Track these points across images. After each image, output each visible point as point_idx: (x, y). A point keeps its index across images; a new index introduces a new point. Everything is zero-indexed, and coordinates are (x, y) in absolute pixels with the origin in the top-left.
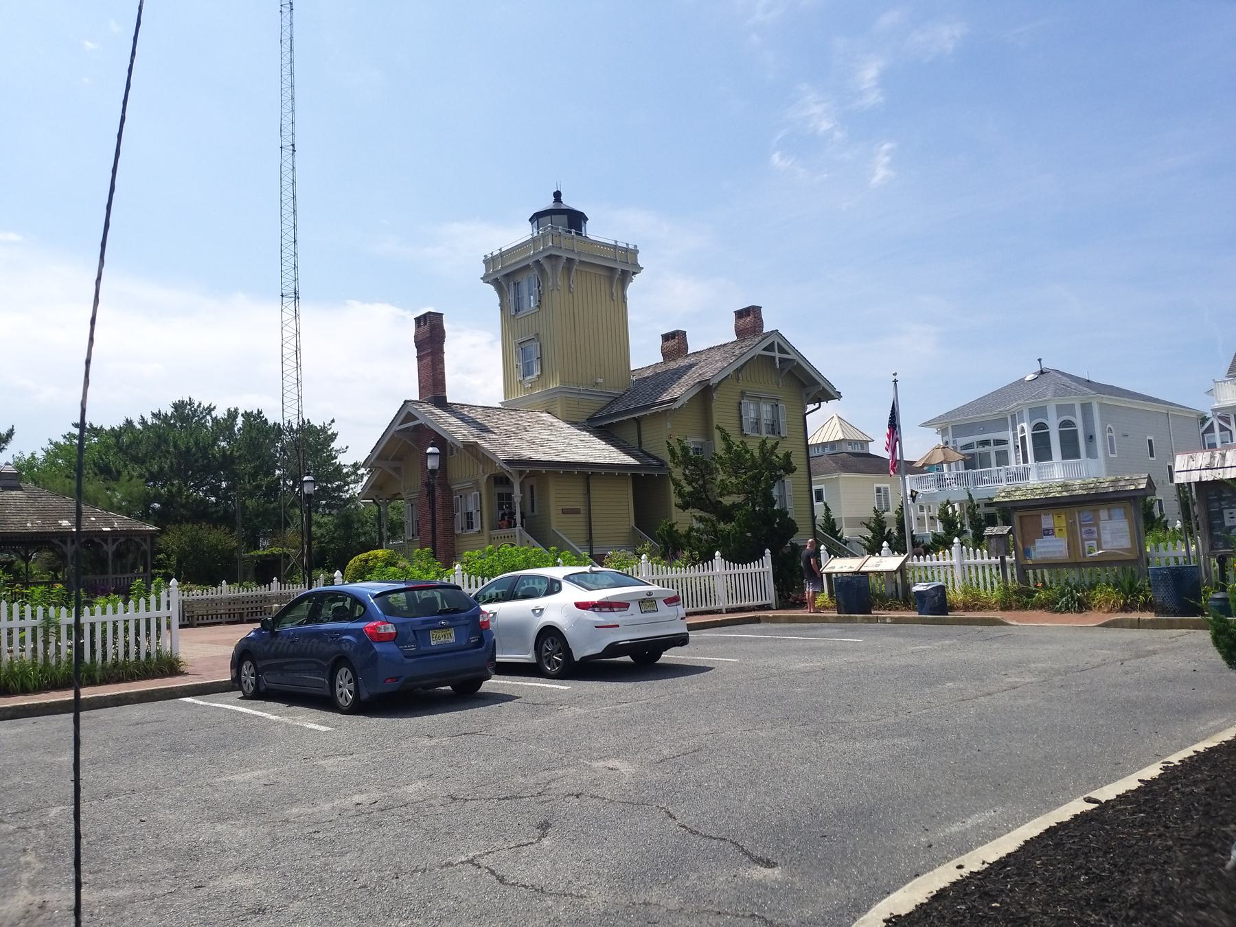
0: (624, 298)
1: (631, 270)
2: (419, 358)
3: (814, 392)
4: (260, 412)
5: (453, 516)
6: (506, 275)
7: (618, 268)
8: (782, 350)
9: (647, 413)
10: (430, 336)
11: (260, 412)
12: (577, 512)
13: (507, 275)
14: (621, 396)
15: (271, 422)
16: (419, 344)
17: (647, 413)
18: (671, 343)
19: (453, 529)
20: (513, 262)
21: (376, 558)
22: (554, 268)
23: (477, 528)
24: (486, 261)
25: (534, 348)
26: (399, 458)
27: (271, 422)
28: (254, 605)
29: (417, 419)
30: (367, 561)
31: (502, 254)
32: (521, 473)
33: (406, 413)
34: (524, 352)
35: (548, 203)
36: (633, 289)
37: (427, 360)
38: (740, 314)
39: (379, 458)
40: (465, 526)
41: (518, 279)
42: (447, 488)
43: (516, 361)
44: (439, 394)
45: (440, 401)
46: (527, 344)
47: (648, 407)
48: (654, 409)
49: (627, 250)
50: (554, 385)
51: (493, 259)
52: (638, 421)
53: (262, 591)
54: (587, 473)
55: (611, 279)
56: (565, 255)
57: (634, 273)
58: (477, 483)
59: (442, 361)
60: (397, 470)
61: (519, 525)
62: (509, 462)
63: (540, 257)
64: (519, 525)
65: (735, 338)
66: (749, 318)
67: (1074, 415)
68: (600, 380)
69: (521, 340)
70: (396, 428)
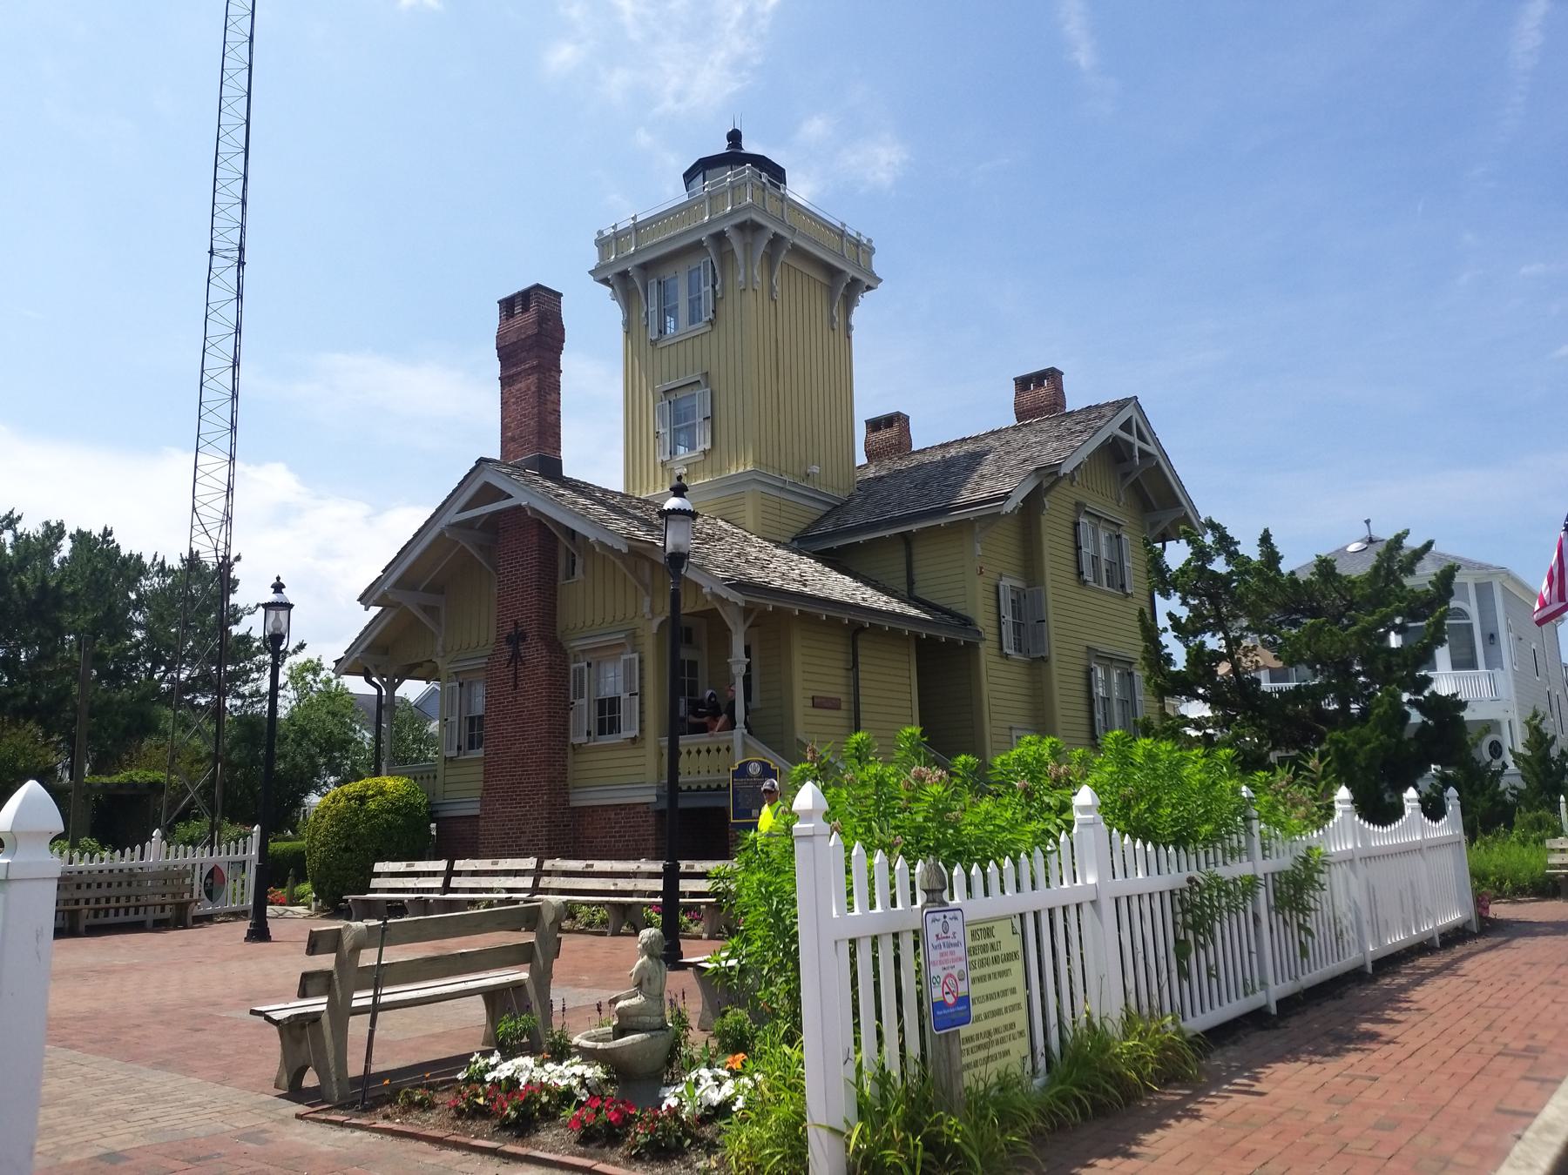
0: (849, 327)
1: (867, 282)
2: (506, 381)
3: (1166, 519)
4: (107, 533)
5: (568, 707)
6: (641, 271)
7: (838, 275)
8: (1141, 437)
9: (942, 521)
10: (530, 338)
11: (107, 533)
12: (834, 705)
13: (645, 267)
14: (845, 504)
15: (124, 552)
16: (507, 353)
17: (942, 521)
18: (884, 434)
19: (565, 733)
20: (658, 243)
21: (382, 792)
22: (747, 247)
23: (626, 734)
24: (603, 243)
25: (700, 402)
26: (436, 588)
27: (124, 552)
28: (104, 892)
29: (510, 496)
30: (362, 799)
31: (637, 227)
32: (747, 611)
33: (479, 485)
34: (671, 401)
35: (721, 147)
36: (865, 312)
37: (528, 383)
38: (1023, 383)
39: (400, 584)
40: (594, 729)
41: (667, 273)
42: (555, 647)
43: (655, 422)
44: (548, 452)
45: (550, 467)
46: (681, 394)
47: (944, 511)
48: (956, 516)
49: (858, 244)
50: (741, 467)
51: (617, 236)
52: (906, 538)
53: (126, 861)
54: (851, 627)
55: (831, 291)
56: (773, 228)
57: (869, 288)
58: (633, 636)
59: (556, 388)
60: (431, 611)
61: (740, 724)
62: (744, 586)
63: (726, 227)
64: (740, 724)
65: (1014, 422)
66: (1039, 392)
67: (1467, 601)
68: (816, 469)
69: (669, 385)
70: (453, 517)
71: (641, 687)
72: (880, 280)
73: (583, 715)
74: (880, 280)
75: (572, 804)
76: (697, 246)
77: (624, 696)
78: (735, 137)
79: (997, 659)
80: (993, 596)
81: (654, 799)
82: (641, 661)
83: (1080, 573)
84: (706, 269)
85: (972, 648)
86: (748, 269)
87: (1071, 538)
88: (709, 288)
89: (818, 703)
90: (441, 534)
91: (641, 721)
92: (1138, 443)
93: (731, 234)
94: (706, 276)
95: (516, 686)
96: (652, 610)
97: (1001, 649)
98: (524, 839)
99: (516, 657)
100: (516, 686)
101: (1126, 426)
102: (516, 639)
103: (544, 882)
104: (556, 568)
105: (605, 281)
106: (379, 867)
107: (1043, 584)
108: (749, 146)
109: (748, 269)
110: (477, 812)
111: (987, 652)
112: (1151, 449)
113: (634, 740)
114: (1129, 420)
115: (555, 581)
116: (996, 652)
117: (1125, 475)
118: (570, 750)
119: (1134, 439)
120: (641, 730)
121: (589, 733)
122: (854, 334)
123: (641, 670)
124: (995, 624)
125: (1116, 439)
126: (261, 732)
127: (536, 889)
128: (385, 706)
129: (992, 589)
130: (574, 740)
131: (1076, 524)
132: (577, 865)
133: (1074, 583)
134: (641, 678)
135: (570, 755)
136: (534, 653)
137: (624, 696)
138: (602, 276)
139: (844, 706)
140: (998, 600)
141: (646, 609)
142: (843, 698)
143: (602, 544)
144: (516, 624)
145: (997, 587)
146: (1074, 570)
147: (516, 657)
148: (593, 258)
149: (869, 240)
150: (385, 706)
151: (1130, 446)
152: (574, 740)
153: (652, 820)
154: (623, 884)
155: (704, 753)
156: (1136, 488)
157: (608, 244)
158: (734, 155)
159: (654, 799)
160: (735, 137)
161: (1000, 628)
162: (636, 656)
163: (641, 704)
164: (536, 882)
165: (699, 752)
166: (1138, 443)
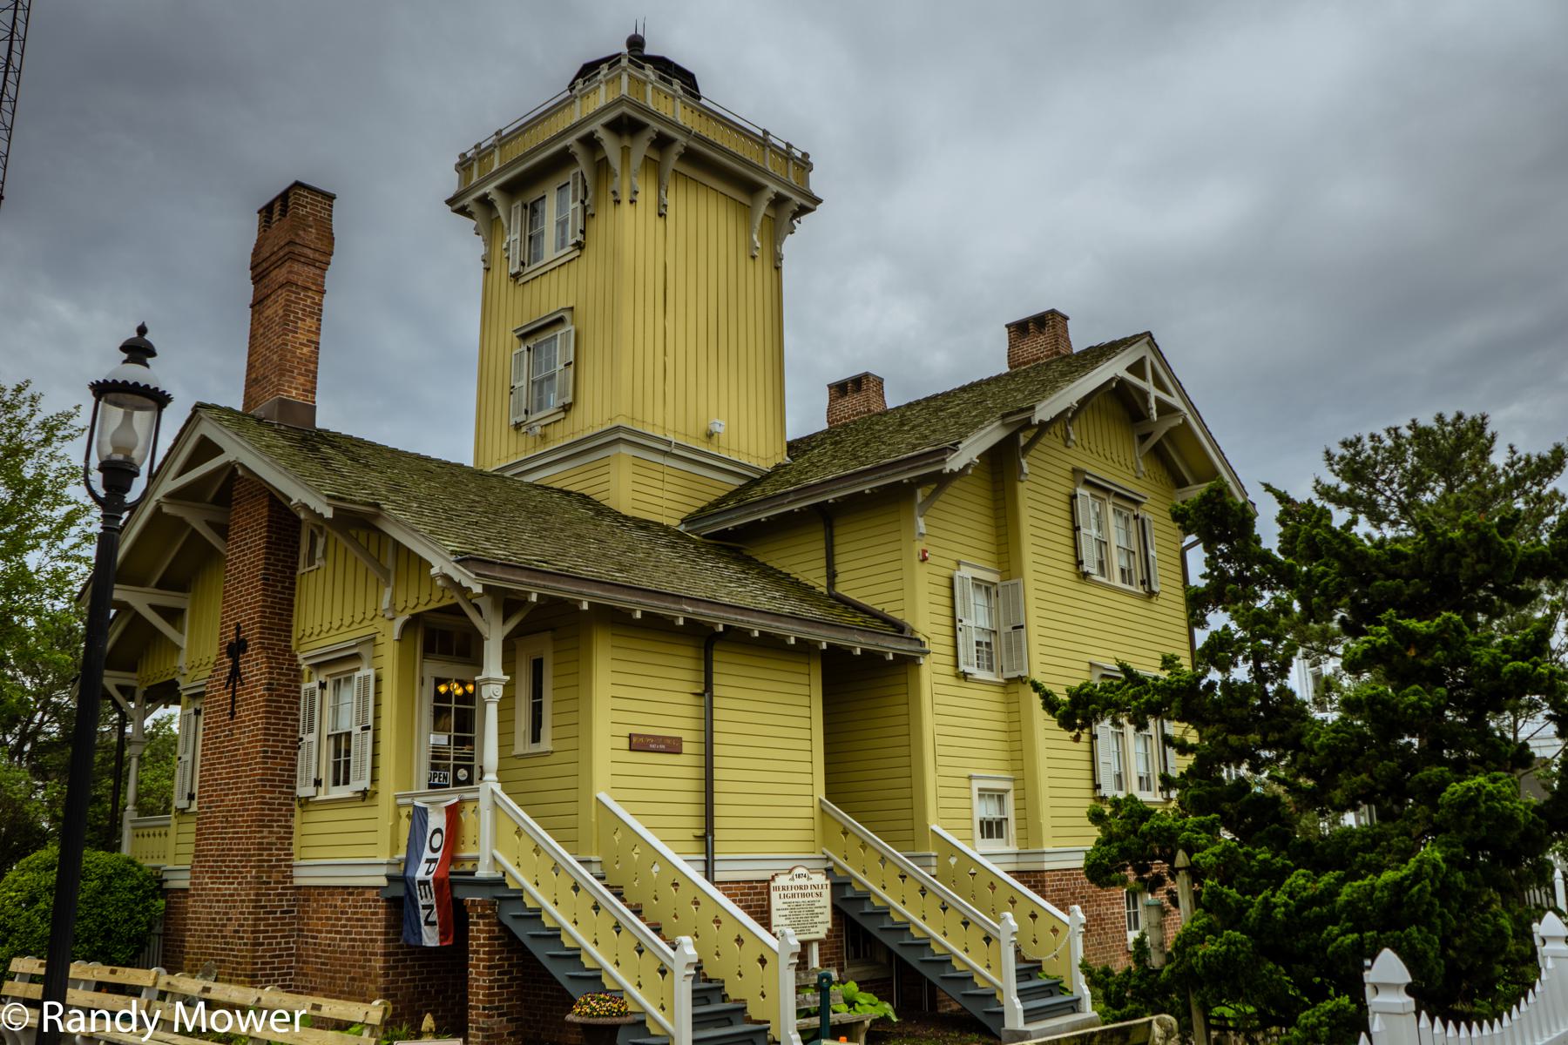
5: (296, 745)
12: (672, 746)
19: (291, 782)
49: (786, 154)
71: (377, 718)
72: (819, 201)
73: (314, 758)
74: (819, 201)
75: (297, 882)
76: (563, 160)
79: (952, 681)
80: (946, 592)
81: (383, 882)
82: (378, 680)
83: (1079, 563)
84: (575, 184)
85: (908, 663)
86: (631, 177)
87: (1067, 516)
88: (578, 204)
89: (639, 744)
90: (158, 509)
91: (374, 768)
92: (1154, 392)
93: (602, 134)
94: (575, 191)
95: (233, 714)
96: (393, 605)
97: (957, 666)
99: (235, 674)
100: (233, 714)
101: (1137, 368)
102: (236, 649)
104: (297, 553)
105: (462, 211)
107: (1020, 574)
109: (631, 177)
111: (932, 674)
112: (1175, 401)
113: (365, 792)
114: (1141, 362)
115: (294, 569)
116: (950, 670)
117: (1144, 438)
119: (1148, 386)
120: (374, 780)
122: (785, 265)
123: (378, 693)
124: (948, 631)
125: (1122, 382)
126: (1331, 750)
128: (1461, 749)
129: (946, 582)
130: (305, 790)
131: (1073, 497)
133: (1073, 577)
134: (377, 705)
135: (298, 810)
136: (255, 668)
137: (356, 730)
138: (457, 206)
139: (686, 747)
140: (953, 598)
141: (385, 604)
142: (686, 736)
143: (305, 507)
144: (238, 628)
145: (952, 580)
146: (1072, 560)
147: (235, 674)
148: (450, 183)
149: (805, 155)
150: (1461, 749)
151: (1144, 395)
152: (305, 790)
156: (1159, 454)
157: (470, 167)
159: (383, 882)
161: (955, 637)
163: (375, 742)
166: (1154, 392)
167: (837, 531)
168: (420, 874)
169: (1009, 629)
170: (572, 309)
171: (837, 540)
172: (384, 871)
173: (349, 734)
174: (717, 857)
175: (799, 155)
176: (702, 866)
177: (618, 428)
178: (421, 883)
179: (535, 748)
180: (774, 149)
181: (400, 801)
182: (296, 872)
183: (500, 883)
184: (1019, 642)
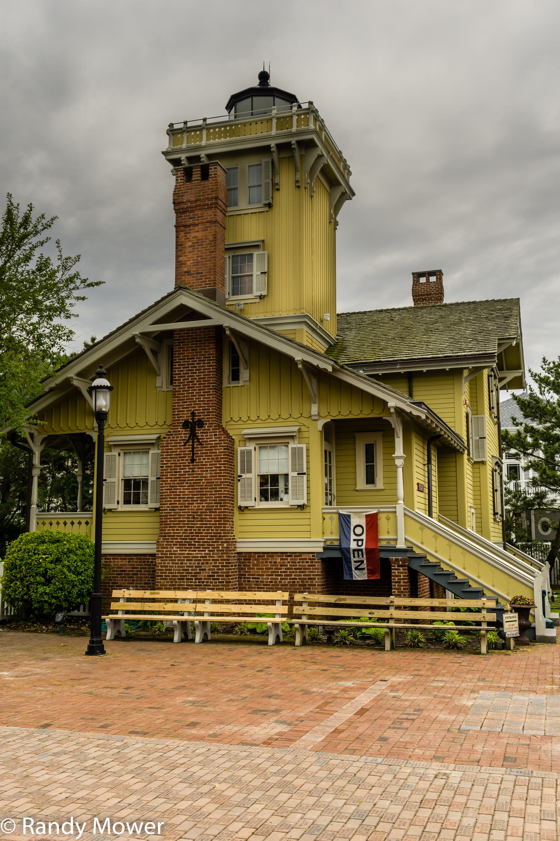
35: (255, 83)
40: (121, 499)
70: (146, 326)
75: (238, 550)
76: (266, 150)
77: (151, 479)
78: (264, 77)
81: (321, 550)
82: (308, 450)
90: (133, 338)
95: (193, 460)
98: (203, 575)
100: (193, 460)
103: (296, 610)
106: (116, 593)
108: (273, 83)
110: (154, 551)
118: (236, 511)
121: (118, 503)
127: (290, 615)
132: (148, 594)
144: (193, 414)
153: (318, 565)
154: (148, 606)
155: (76, 525)
158: (264, 88)
159: (321, 550)
160: (264, 77)
162: (304, 446)
163: (308, 481)
164: (290, 610)
165: (72, 523)
167: (415, 384)
168: (353, 545)
169: (478, 438)
170: (263, 241)
171: (415, 389)
172: (322, 545)
173: (287, 475)
174: (103, 542)
175: (182, 126)
176: (502, 545)
177: (306, 316)
178: (354, 550)
179: (370, 487)
180: (199, 128)
181: (325, 511)
182: (238, 545)
183: (409, 550)
184: (483, 445)
